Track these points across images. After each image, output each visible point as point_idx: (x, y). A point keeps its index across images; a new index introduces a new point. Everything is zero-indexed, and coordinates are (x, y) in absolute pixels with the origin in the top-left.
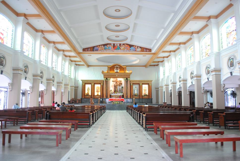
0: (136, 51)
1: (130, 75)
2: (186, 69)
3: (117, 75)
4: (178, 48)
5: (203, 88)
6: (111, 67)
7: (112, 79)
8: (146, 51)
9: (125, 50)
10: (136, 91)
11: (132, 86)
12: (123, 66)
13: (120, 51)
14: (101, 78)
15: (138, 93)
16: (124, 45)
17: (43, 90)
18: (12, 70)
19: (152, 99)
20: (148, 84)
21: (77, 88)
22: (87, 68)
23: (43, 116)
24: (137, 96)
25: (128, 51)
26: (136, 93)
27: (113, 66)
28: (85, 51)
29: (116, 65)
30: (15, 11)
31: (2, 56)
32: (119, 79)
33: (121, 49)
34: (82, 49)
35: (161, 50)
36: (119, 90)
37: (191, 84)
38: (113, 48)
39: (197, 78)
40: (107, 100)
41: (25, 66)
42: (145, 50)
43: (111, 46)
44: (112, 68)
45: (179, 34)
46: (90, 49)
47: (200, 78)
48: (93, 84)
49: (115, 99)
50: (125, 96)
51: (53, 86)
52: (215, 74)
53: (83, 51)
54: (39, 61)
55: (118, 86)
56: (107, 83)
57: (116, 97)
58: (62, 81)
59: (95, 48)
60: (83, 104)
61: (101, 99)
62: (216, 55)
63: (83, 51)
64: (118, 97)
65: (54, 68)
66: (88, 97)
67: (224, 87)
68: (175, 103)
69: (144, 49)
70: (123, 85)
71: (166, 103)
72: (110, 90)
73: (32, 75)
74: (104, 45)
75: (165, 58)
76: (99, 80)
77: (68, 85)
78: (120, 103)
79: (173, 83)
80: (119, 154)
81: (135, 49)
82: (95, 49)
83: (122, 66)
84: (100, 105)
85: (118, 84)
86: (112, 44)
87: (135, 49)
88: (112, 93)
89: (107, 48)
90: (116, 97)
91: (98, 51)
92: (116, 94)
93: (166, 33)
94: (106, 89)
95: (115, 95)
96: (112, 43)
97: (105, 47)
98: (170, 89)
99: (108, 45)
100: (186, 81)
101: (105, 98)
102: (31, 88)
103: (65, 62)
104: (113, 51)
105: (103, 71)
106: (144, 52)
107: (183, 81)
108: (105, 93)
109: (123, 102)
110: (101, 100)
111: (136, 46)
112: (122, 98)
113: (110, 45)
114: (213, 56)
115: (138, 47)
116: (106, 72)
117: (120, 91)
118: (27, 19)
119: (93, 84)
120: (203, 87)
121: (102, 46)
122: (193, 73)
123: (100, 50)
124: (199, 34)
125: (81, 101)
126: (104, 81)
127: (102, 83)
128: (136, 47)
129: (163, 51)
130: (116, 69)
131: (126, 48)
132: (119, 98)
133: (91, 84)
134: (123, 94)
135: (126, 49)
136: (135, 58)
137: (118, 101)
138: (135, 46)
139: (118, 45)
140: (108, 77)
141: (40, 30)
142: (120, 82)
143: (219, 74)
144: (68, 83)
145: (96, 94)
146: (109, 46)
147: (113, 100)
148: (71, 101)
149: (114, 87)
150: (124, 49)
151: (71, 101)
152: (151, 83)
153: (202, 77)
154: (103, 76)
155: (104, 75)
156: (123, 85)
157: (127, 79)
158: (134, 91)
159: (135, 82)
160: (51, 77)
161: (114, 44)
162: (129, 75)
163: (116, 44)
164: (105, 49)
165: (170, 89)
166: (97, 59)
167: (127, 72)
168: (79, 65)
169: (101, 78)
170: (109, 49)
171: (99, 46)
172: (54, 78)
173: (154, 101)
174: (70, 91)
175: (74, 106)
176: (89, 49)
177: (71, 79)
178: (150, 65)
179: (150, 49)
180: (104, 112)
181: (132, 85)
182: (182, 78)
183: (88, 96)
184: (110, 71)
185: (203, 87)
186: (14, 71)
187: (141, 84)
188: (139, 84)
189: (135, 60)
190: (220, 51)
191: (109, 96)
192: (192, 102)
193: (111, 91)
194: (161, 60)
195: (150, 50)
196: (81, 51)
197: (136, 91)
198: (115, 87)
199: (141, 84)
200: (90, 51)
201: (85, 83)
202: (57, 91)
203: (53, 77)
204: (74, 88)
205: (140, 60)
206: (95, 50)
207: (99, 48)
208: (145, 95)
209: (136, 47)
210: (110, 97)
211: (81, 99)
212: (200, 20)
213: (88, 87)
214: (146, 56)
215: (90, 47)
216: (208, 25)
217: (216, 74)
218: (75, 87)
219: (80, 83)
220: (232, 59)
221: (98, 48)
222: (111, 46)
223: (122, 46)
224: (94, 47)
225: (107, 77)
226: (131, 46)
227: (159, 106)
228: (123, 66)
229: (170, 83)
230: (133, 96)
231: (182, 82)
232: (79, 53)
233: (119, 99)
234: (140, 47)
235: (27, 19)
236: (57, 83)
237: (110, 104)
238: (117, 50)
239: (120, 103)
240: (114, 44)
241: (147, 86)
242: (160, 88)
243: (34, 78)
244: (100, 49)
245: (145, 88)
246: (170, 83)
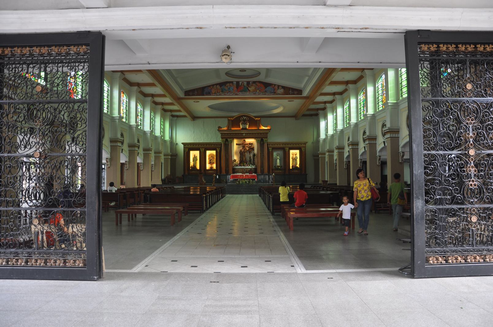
1: (268, 133)
2: (375, 116)
3: (245, 133)
4: (346, 90)
5: (402, 154)
6: (235, 119)
7: (235, 141)
8: (294, 94)
9: (257, 91)
10: (278, 161)
12: (254, 118)
13: (248, 94)
14: (217, 139)
15: (283, 165)
17: (124, 162)
19: (307, 175)
21: (175, 157)
22: (192, 121)
23: (394, 137)
24: (280, 170)
25: (262, 94)
27: (238, 117)
28: (189, 95)
29: (242, 116)
30: (128, 80)
32: (248, 141)
33: (249, 91)
35: (317, 91)
36: (248, 159)
37: (383, 145)
38: (235, 89)
39: (370, 141)
40: (230, 178)
42: (290, 91)
43: (233, 85)
44: (235, 122)
45: (329, 84)
46: (197, 91)
47: (374, 141)
48: (203, 149)
49: (241, 176)
50: (259, 170)
51: (122, 152)
52: (390, 137)
53: (185, 95)
54: (118, 118)
55: (246, 153)
56: (227, 147)
57: (244, 171)
60: (187, 185)
61: (217, 176)
62: (392, 107)
63: (185, 95)
64: (247, 173)
65: (123, 118)
66: (195, 172)
67: (403, 156)
70: (256, 151)
71: (327, 181)
72: (233, 159)
73: (109, 140)
74: (221, 84)
75: (327, 104)
76: (214, 143)
77: (160, 153)
78: (249, 182)
79: (391, 131)
81: (274, 90)
82: (205, 92)
83: (253, 117)
84: (216, 186)
85: (247, 149)
87: (274, 90)
88: (237, 166)
89: (227, 89)
90: (243, 173)
91: (210, 94)
92: (243, 167)
93: (317, 74)
94: (225, 159)
95: (241, 169)
97: (222, 87)
98: (346, 155)
99: (228, 84)
101: (225, 174)
102: (108, 160)
103: (155, 114)
104: (236, 95)
105: (219, 127)
106: (289, 94)
107: (352, 146)
108: (224, 165)
109: (254, 181)
110: (218, 177)
111: (275, 85)
112: (253, 174)
113: (231, 84)
114: (388, 109)
115: (279, 86)
116: (225, 128)
117: (250, 161)
118: (124, 74)
119: (202, 150)
120: (403, 152)
122: (385, 125)
124: (333, 103)
125: (182, 180)
126: (221, 144)
127: (218, 148)
128: (276, 86)
130: (242, 124)
132: (248, 174)
134: (256, 166)
135: (258, 91)
136: (274, 105)
137: (247, 179)
138: (273, 86)
139: (245, 83)
140: (230, 138)
141: (150, 94)
142: (250, 145)
143: (396, 136)
144: (150, 146)
145: (208, 166)
147: (237, 177)
148: (167, 180)
149: (239, 154)
150: (254, 92)
151: (167, 180)
152: (305, 147)
153: (400, 133)
154: (220, 135)
155: (221, 133)
156: (256, 151)
157: (262, 140)
158: (274, 161)
159: (276, 146)
162: (266, 132)
163: (240, 83)
164: (222, 92)
165: (346, 155)
166: (210, 107)
167: (263, 128)
168: (177, 116)
169: (217, 139)
170: (229, 92)
172: (123, 138)
173: (311, 178)
174: (120, 153)
175: (173, 187)
176: (196, 92)
177: (165, 141)
178: (304, 115)
180: (222, 196)
181: (271, 150)
182: (388, 125)
183: (195, 170)
184: (233, 127)
185: (403, 152)
186: (130, 148)
187: (287, 149)
188: (283, 149)
189: (276, 108)
190: (399, 101)
191: (231, 171)
193: (235, 161)
194: (322, 106)
195: (300, 92)
196: (181, 94)
197: (278, 161)
198: (242, 154)
199: (288, 148)
200: (197, 95)
201: (189, 147)
202: (144, 164)
203: (122, 135)
204: (170, 157)
205: (284, 107)
206: (205, 93)
208: (294, 167)
210: (234, 172)
211: (183, 176)
213: (195, 154)
214: (293, 101)
215: (197, 89)
216: (364, 77)
217: (392, 136)
218: (171, 156)
219: (181, 147)
222: (233, 85)
225: (227, 138)
226: (267, 85)
227: (312, 186)
228: (256, 117)
229: (346, 143)
230: (272, 170)
231: (367, 142)
232: (178, 99)
233: (248, 176)
234: (283, 87)
235: (124, 74)
236: (144, 150)
237: (233, 184)
239: (249, 182)
240: (238, 83)
241: (297, 152)
242: (320, 156)
243: (130, 149)
244: (213, 91)
245: (295, 154)
246: (346, 143)
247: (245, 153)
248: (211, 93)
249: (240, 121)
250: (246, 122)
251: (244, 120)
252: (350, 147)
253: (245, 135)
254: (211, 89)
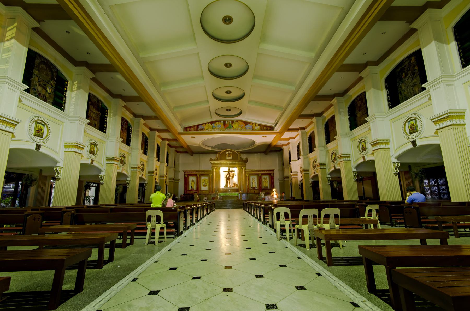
0: (253, 129)
8: (267, 130)
16: (237, 123)
18: (64, 146)
20: (269, 174)
26: (254, 186)
28: (187, 131)
31: (93, 143)
34: (183, 128)
41: (91, 144)
42: (265, 128)
43: (221, 123)
46: (193, 128)
53: (184, 131)
58: (166, 174)
59: (200, 127)
63: (184, 131)
68: (14, 186)
69: (264, 127)
80: (234, 290)
86: (222, 122)
87: (253, 127)
91: (203, 130)
96: (222, 119)
97: (213, 125)
99: (217, 123)
100: (308, 171)
104: (223, 130)
106: (264, 130)
111: (253, 123)
113: (219, 122)
115: (256, 124)
121: (210, 124)
123: (207, 129)
128: (254, 124)
129: (271, 151)
131: (240, 126)
133: (196, 175)
138: (252, 124)
139: (230, 122)
146: (219, 124)
160: (154, 169)
161: (224, 122)
163: (227, 122)
170: (218, 128)
171: (205, 124)
179: (272, 127)
188: (257, 174)
192: (66, 209)
203: (156, 170)
207: (205, 127)
209: (254, 125)
212: (328, 94)
220: (334, 154)
221: (204, 127)
223: (235, 124)
224: (198, 126)
234: (259, 125)
238: (229, 129)
240: (224, 122)
244: (206, 128)
248: (204, 129)
251: (229, 154)
252: (303, 173)
254: (204, 126)
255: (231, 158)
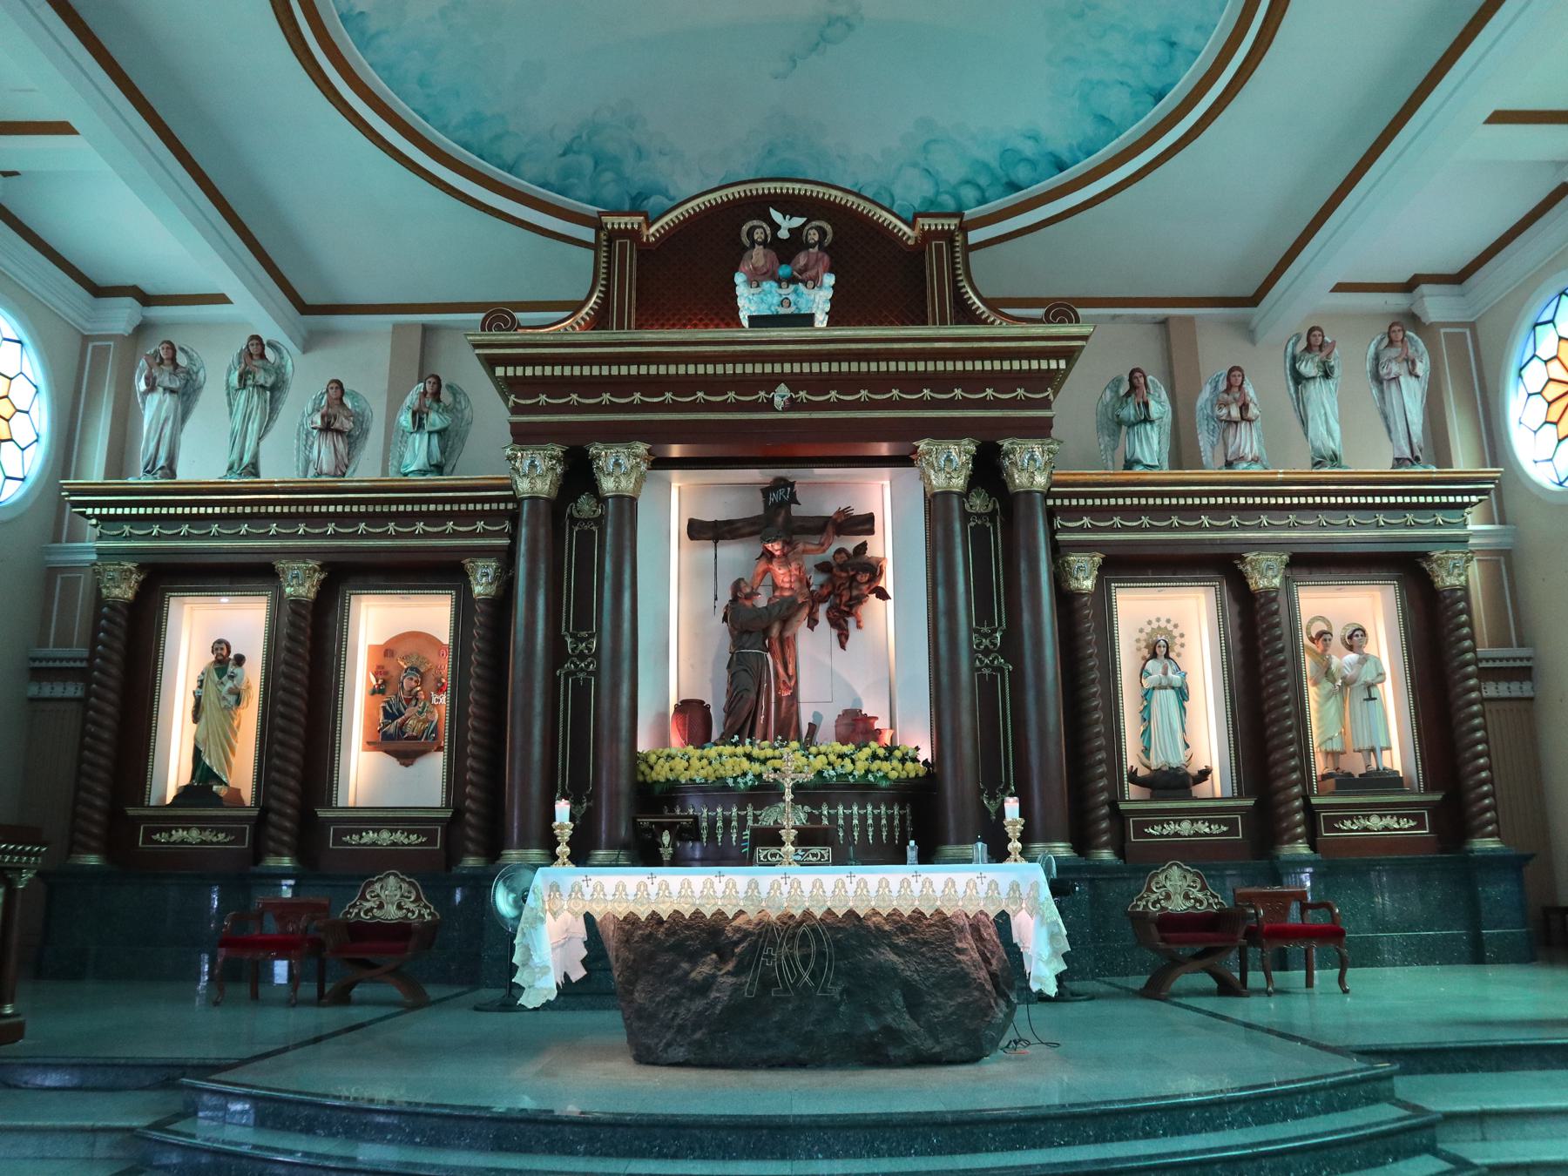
3: (795, 382)
11: (1103, 603)
29: (758, 206)
247: (785, 622)
249: (734, 256)
250: (802, 259)
251: (786, 250)
253: (793, 405)
255: (818, 300)
